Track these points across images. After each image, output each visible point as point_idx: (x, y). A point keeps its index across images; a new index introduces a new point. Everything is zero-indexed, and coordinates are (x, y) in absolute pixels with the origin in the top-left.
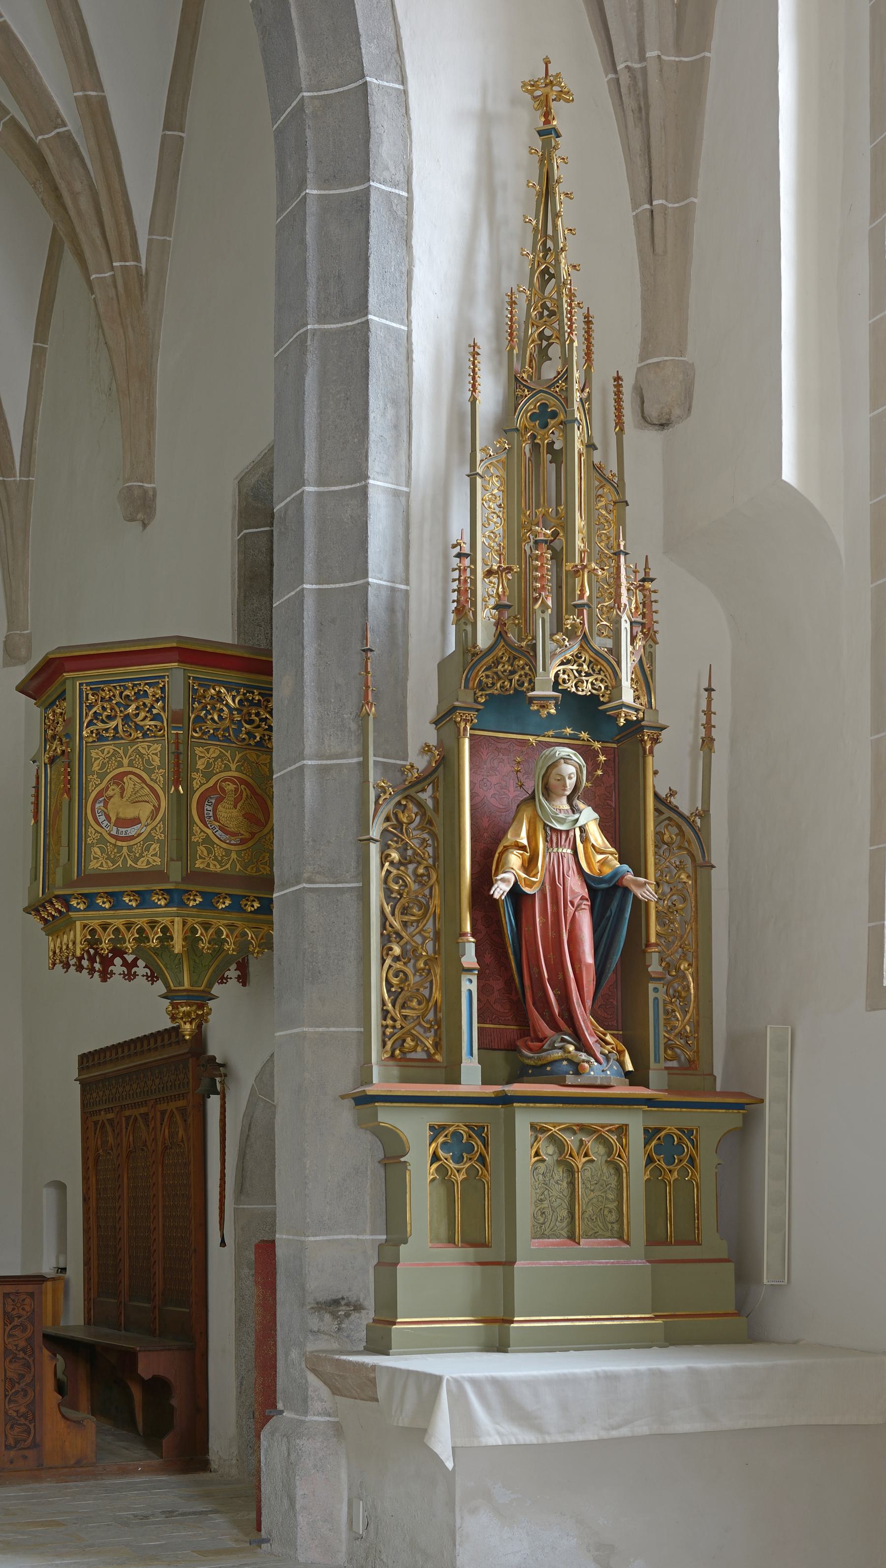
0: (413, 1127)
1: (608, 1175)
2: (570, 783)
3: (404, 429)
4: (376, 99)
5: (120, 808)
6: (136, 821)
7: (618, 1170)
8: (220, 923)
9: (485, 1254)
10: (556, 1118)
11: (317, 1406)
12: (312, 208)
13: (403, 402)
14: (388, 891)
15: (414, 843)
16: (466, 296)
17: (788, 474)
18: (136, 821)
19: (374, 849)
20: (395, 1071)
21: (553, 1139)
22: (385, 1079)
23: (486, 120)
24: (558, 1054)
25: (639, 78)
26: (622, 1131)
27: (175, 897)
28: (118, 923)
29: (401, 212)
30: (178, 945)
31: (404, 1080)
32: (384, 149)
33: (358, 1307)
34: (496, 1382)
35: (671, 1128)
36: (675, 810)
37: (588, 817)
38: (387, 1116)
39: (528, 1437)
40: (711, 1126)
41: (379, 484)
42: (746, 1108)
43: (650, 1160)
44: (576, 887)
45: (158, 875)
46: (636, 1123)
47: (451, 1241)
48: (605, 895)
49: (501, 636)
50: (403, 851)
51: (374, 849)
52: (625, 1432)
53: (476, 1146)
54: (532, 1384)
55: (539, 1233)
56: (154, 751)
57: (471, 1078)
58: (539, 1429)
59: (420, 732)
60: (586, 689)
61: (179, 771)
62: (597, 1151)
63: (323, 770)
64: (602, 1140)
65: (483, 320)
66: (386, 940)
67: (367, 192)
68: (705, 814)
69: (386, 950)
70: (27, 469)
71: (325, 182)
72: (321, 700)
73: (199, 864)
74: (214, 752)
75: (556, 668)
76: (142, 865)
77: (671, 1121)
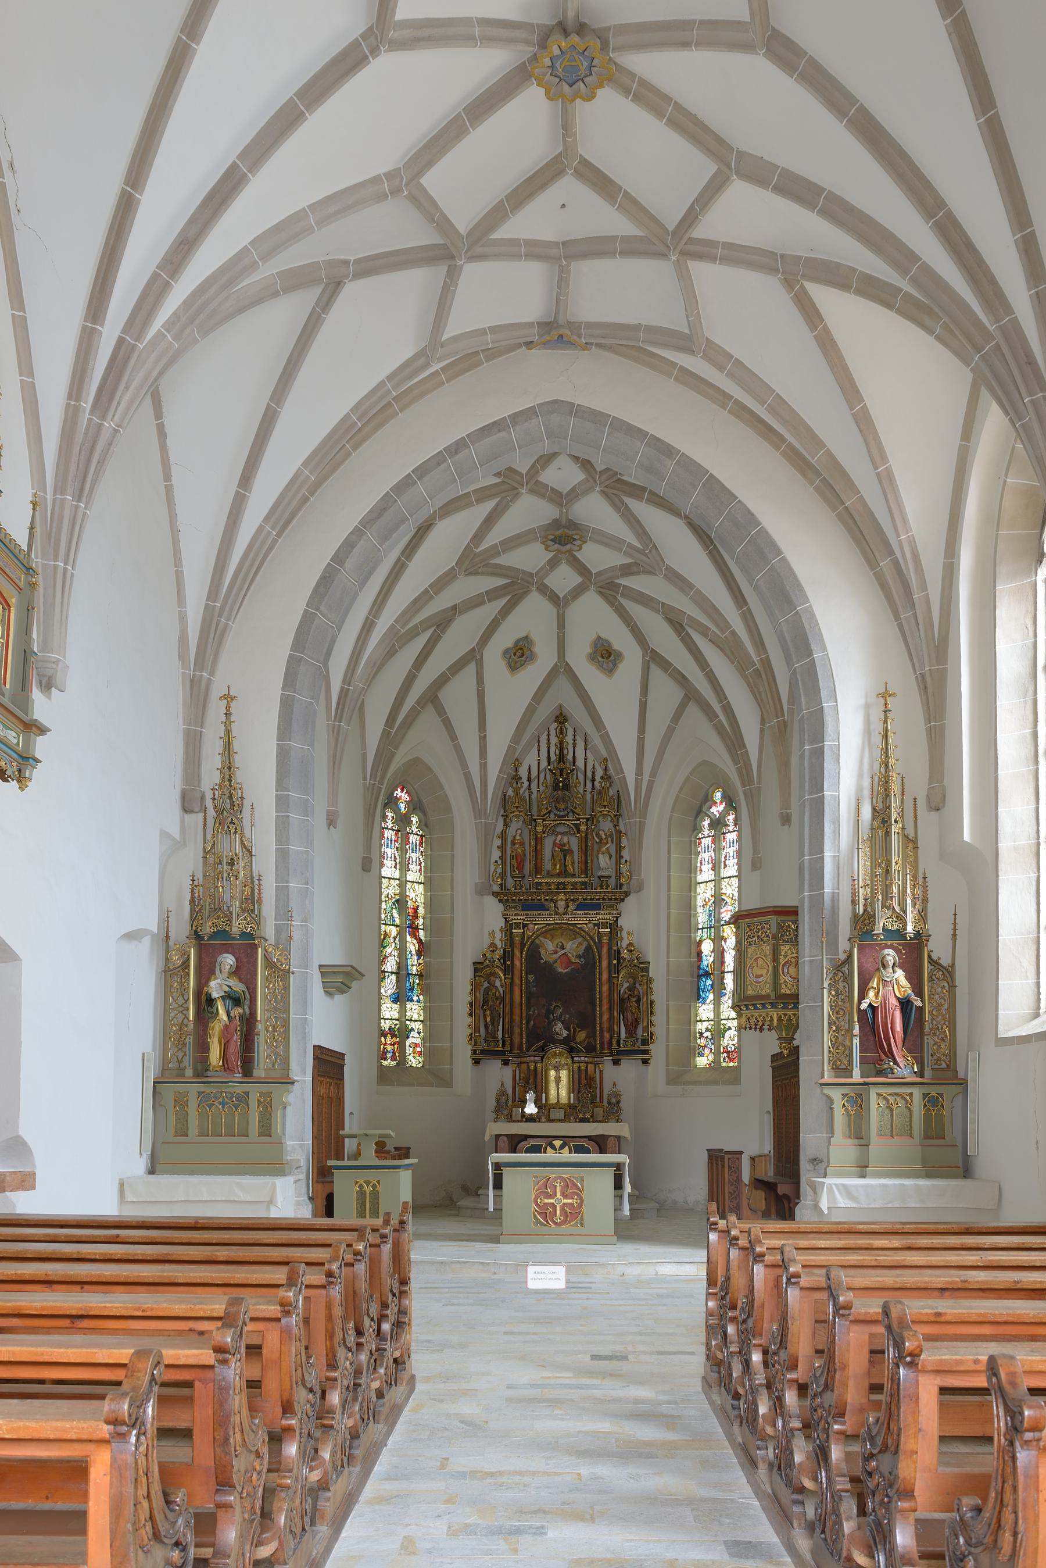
0: (836, 1094)
1: (906, 1112)
2: (891, 963)
3: (837, 832)
4: (826, 711)
5: (757, 971)
6: (762, 976)
7: (910, 1110)
8: (790, 1013)
9: (862, 1142)
10: (885, 1090)
11: (810, 1198)
12: (807, 753)
13: (836, 822)
14: (831, 1006)
15: (841, 988)
16: (860, 775)
17: (967, 837)
18: (762, 976)
19: (825, 991)
20: (833, 1073)
21: (885, 1098)
22: (829, 1077)
23: (867, 706)
24: (886, 1066)
25: (923, 675)
26: (911, 1095)
27: (773, 1005)
28: (756, 1015)
29: (835, 751)
30: (775, 1022)
31: (836, 1077)
32: (829, 729)
33: (822, 1161)
34: (844, 1185)
35: (933, 1093)
36: (940, 965)
37: (900, 974)
38: (828, 1091)
39: (855, 1205)
40: (948, 1091)
41: (828, 854)
42: (964, 1083)
43: (925, 1105)
44: (894, 1002)
45: (768, 997)
46: (917, 1093)
47: (850, 1137)
48: (905, 1004)
49: (865, 910)
50: (837, 991)
51: (825, 991)
52: (890, 1205)
53: (858, 1101)
54: (856, 1186)
55: (880, 1135)
56: (767, 949)
57: (857, 1076)
58: (858, 1202)
59: (843, 944)
60: (895, 927)
61: (775, 958)
62: (901, 1103)
63: (811, 961)
64: (903, 1098)
65: (866, 783)
66: (830, 1024)
67: (823, 746)
68: (953, 965)
69: (830, 1028)
70: (759, 782)
71: (811, 743)
72: (811, 936)
73: (783, 991)
74: (788, 947)
75: (882, 921)
76: (763, 993)
77: (934, 1091)
